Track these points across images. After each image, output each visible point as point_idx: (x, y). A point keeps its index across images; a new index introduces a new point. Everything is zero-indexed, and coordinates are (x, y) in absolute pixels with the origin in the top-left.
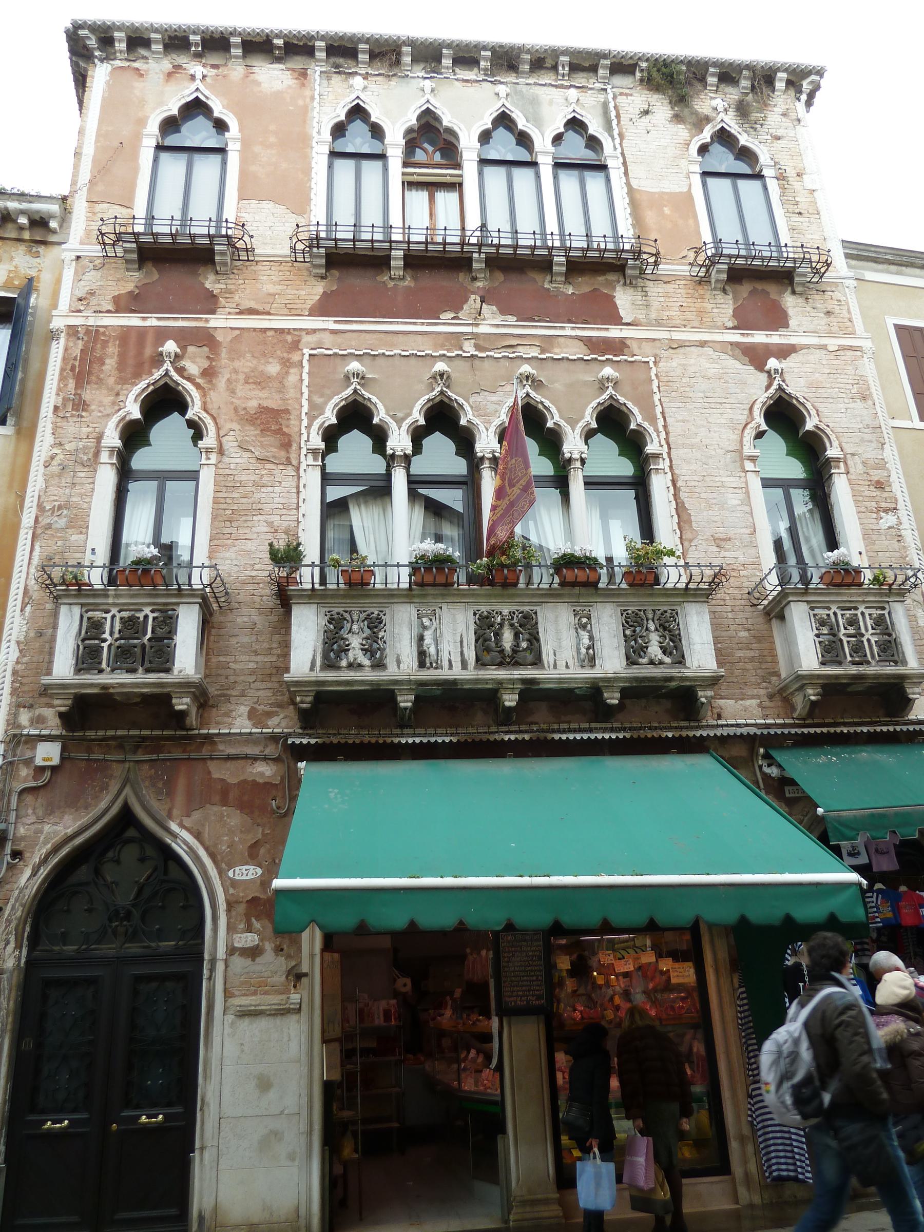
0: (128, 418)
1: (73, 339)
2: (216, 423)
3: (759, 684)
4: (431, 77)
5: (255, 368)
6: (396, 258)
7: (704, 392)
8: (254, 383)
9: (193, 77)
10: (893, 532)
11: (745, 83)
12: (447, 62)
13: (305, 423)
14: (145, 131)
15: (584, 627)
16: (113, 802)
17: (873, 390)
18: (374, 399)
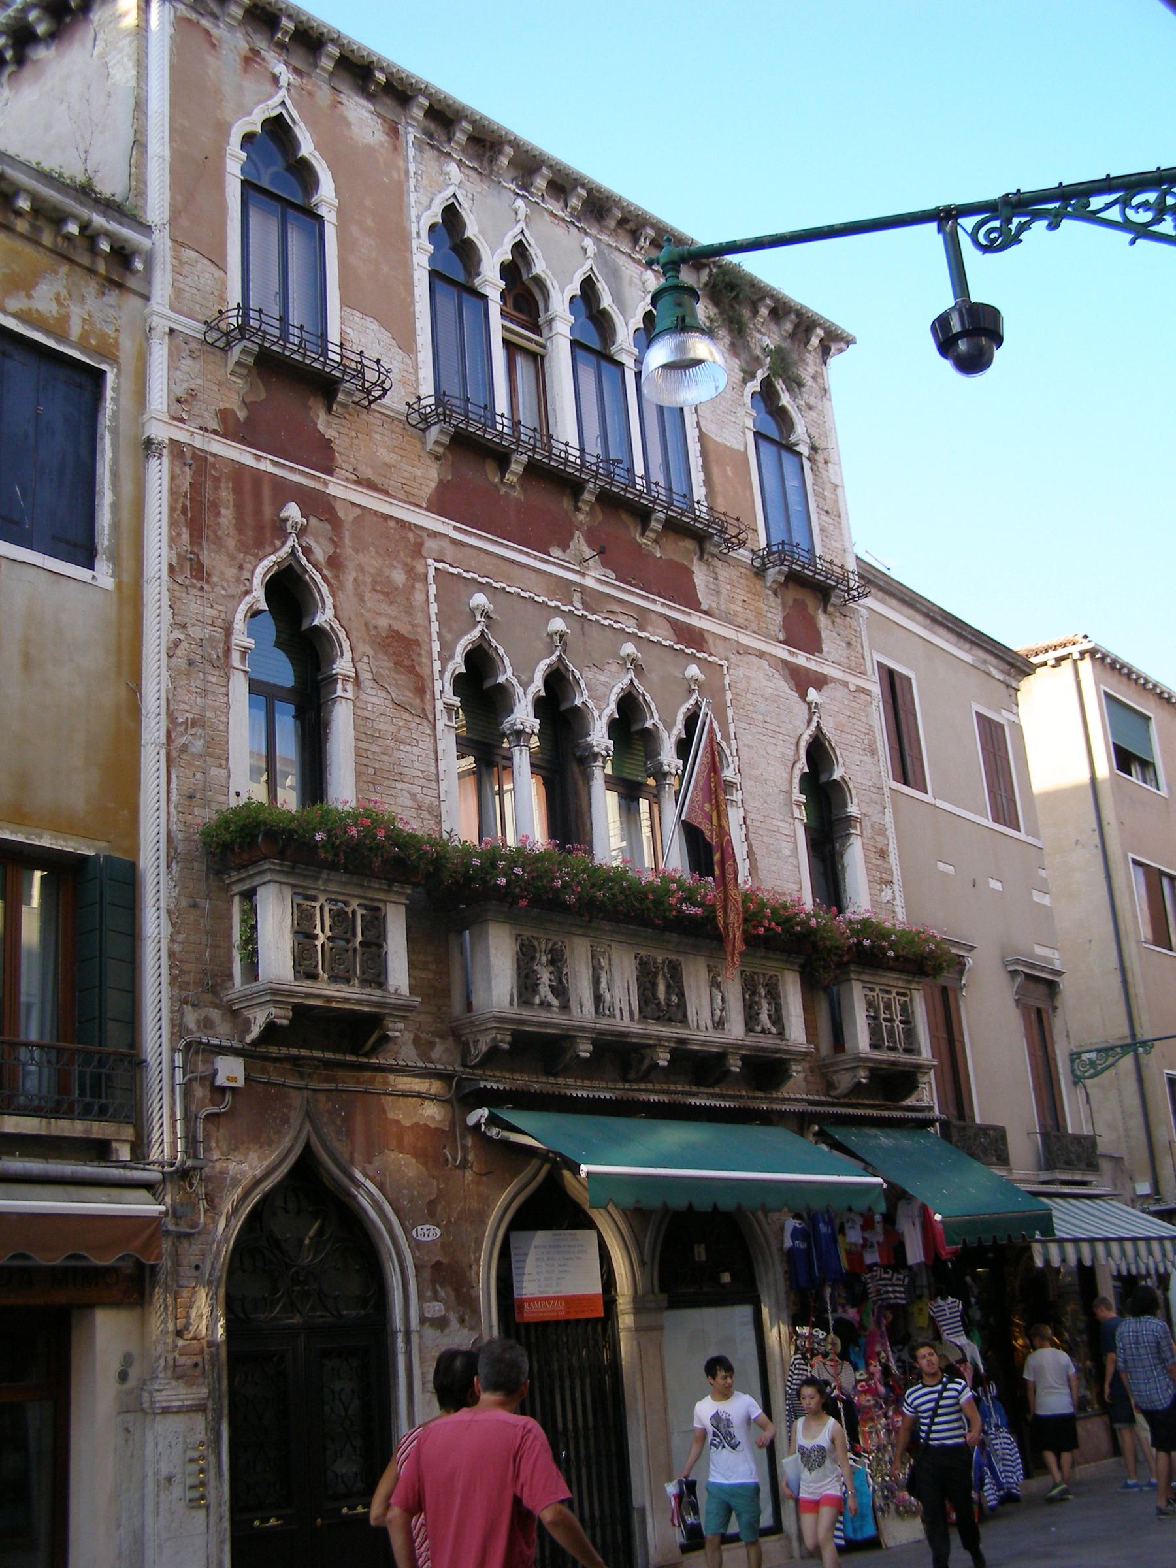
8: (382, 592)
11: (788, 326)
12: (540, 183)
15: (718, 986)
16: (296, 1138)
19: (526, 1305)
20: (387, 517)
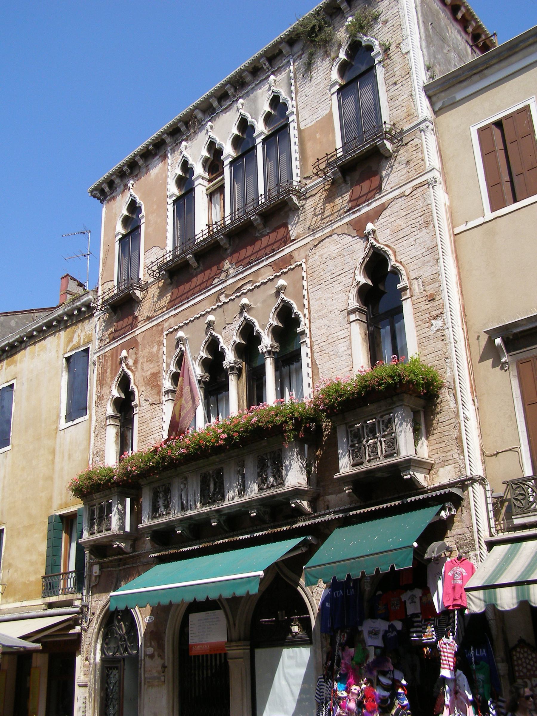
19: (193, 648)
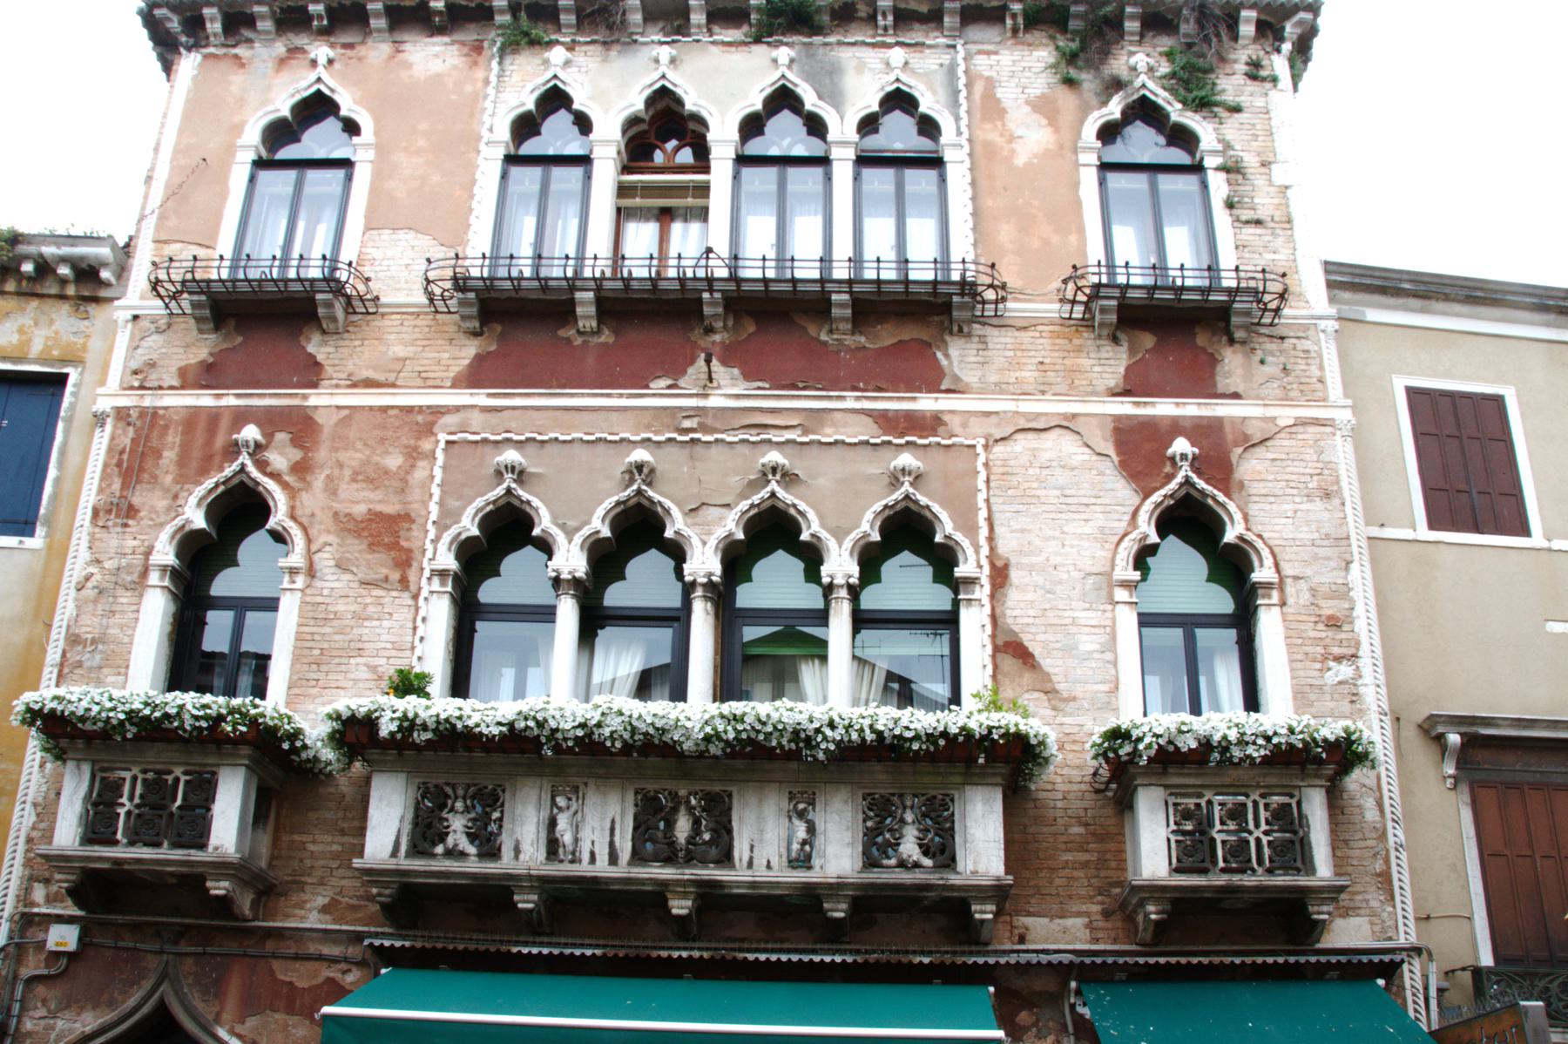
0: (187, 529)
1: (121, 425)
2: (307, 534)
3: (1091, 897)
4: (674, 42)
5: (369, 462)
6: (583, 303)
7: (1062, 488)
9: (314, 63)
10: (1346, 689)
13: (432, 535)
14: (240, 142)
15: (801, 815)
17: (1344, 484)
18: (536, 502)
20: (384, 409)
